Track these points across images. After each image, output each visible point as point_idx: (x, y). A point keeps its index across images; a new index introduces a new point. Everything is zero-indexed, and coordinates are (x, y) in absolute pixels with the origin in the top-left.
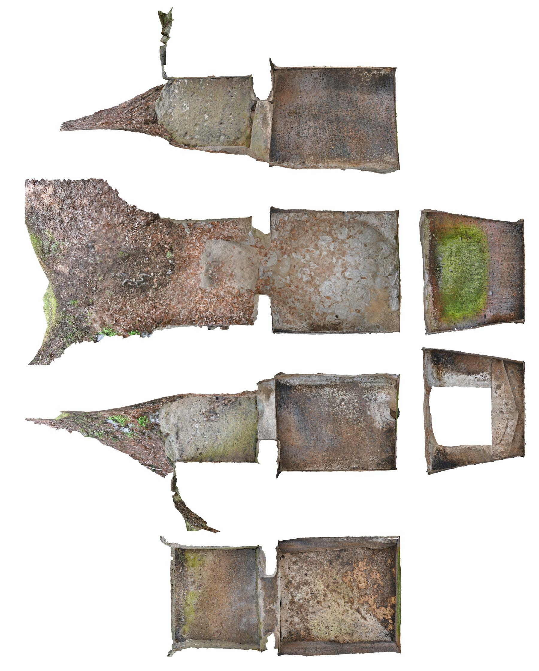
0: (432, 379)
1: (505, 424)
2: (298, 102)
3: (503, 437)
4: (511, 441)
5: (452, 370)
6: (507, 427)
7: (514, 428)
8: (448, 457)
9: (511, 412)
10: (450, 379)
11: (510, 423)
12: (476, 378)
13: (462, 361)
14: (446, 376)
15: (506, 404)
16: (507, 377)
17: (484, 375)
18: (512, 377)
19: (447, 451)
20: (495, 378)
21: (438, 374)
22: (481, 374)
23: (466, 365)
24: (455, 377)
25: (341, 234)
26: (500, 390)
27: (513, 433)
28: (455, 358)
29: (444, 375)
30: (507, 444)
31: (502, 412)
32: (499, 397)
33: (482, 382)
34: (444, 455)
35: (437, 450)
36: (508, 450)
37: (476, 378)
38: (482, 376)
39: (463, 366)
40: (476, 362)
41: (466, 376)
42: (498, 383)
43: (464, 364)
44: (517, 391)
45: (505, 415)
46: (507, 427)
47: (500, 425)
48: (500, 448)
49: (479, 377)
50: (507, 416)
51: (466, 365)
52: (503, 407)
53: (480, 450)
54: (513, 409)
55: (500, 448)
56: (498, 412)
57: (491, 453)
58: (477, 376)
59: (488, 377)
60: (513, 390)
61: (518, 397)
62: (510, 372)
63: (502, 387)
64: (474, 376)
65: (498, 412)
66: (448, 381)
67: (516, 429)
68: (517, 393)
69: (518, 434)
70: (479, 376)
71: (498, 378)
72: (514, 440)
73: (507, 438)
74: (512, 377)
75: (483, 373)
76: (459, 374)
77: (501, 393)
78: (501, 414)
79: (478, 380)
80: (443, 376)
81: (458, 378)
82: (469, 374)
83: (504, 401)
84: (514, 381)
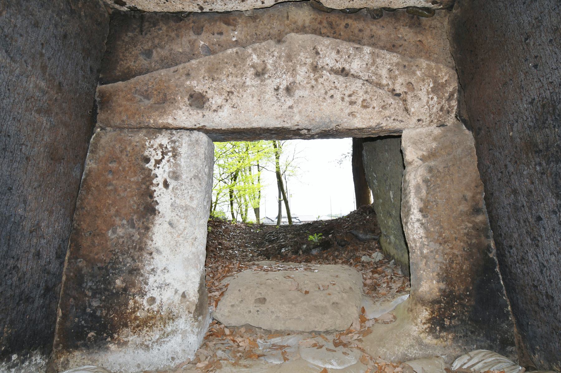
0: (165, 348)
1: (333, 77)
2: (534, 94)
3: (379, 85)
4: (394, 58)
5: (135, 271)
6: (343, 72)
7: (347, 48)
8: (459, 289)
9: (289, 58)
10: (168, 277)
11: (329, 59)
12: (166, 185)
13: (102, 235)
14: (155, 293)
15: (260, 74)
16: (163, 72)
17: (156, 155)
18: (164, 53)
19: (436, 294)
20: (163, 113)
21: (147, 323)
22: (151, 165)
23: (117, 221)
24: (159, 261)
25: (184, 295)
26: (210, 93)
27: (367, 50)
28: (91, 262)
29: (152, 300)
30: (406, 69)
31: (288, 90)
32: (235, 99)
33: (182, 161)
34: (450, 305)
35: (431, 331)
36: (429, 67)
37: (166, 185)
38: (158, 162)
39: (120, 232)
40: (107, 183)
41: (158, 220)
42: (183, 101)
43: (112, 226)
44: (215, 39)
45: (299, 78)
46: (343, 72)
47: (338, 96)
48: (423, 95)
49: (161, 173)
50: (302, 71)
51: (117, 221)
52: (271, 84)
53: (430, 170)
54: (277, 50)
55: (423, 95)
56: (290, 102)
57: (437, 131)
58: (160, 180)
59: (163, 139)
60: (210, 51)
61: (235, 35)
62: (143, 62)
63: (199, 88)
64: (159, 191)
65: (290, 102)
66: (177, 286)
67: (349, 40)
68: (223, 38)
69: (367, 32)
70: (157, 172)
71: (165, 101)
72: (392, 48)
73: (384, 72)
74: (164, 53)
75: (147, 160)
76: (151, 246)
77: (220, 91)
78: (298, 93)
79: (176, 176)
80: (155, 307)
81: (166, 251)
82: (149, 209)
83: (250, 80)
84: (179, 47)
